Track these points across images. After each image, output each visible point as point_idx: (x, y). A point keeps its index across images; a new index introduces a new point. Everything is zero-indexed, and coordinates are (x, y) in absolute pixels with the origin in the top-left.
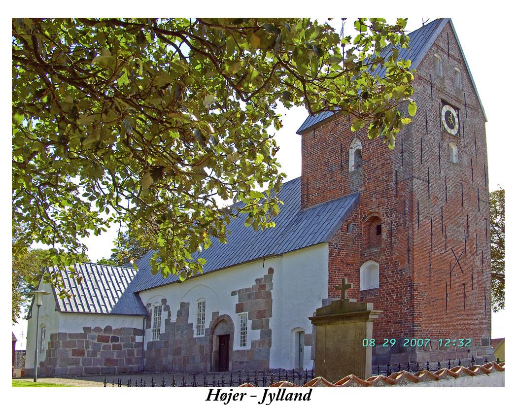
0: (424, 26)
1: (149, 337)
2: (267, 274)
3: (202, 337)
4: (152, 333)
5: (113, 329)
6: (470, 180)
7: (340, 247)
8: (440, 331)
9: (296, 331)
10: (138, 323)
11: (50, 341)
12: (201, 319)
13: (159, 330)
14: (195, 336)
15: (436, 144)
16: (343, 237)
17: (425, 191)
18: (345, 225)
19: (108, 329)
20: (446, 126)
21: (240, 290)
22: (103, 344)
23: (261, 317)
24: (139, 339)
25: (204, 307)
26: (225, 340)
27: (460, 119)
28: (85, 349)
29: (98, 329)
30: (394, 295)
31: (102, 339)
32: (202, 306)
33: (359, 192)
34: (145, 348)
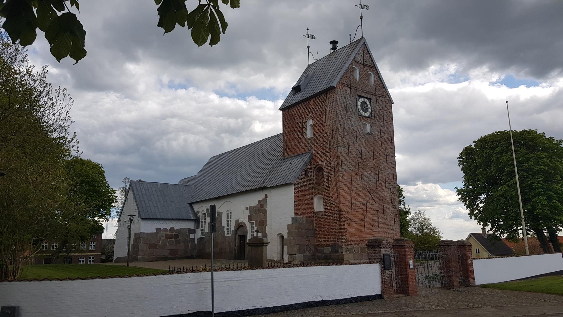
0: (351, 43)
1: (199, 234)
2: (264, 198)
3: (230, 236)
4: (200, 232)
5: (175, 229)
7: (301, 185)
9: (280, 235)
10: (190, 225)
11: (134, 238)
12: (229, 222)
13: (204, 230)
14: (226, 235)
18: (304, 172)
19: (172, 229)
20: (361, 111)
21: (250, 206)
23: (262, 224)
24: (192, 236)
25: (231, 216)
26: (243, 237)
27: (372, 105)
29: (165, 230)
30: (331, 217)
32: (229, 215)
33: (312, 151)
34: (196, 242)
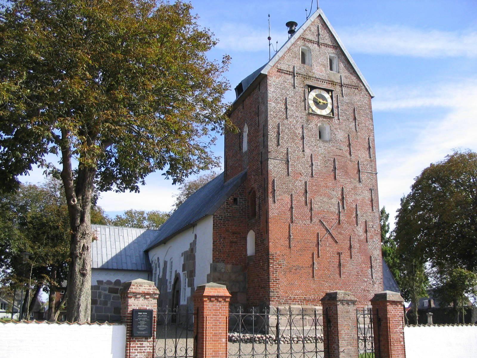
6: (347, 154)
8: (305, 298)
15: (299, 126)
16: (229, 210)
17: (284, 169)
22: (113, 295)
28: (97, 298)
29: (109, 282)
31: (112, 291)
